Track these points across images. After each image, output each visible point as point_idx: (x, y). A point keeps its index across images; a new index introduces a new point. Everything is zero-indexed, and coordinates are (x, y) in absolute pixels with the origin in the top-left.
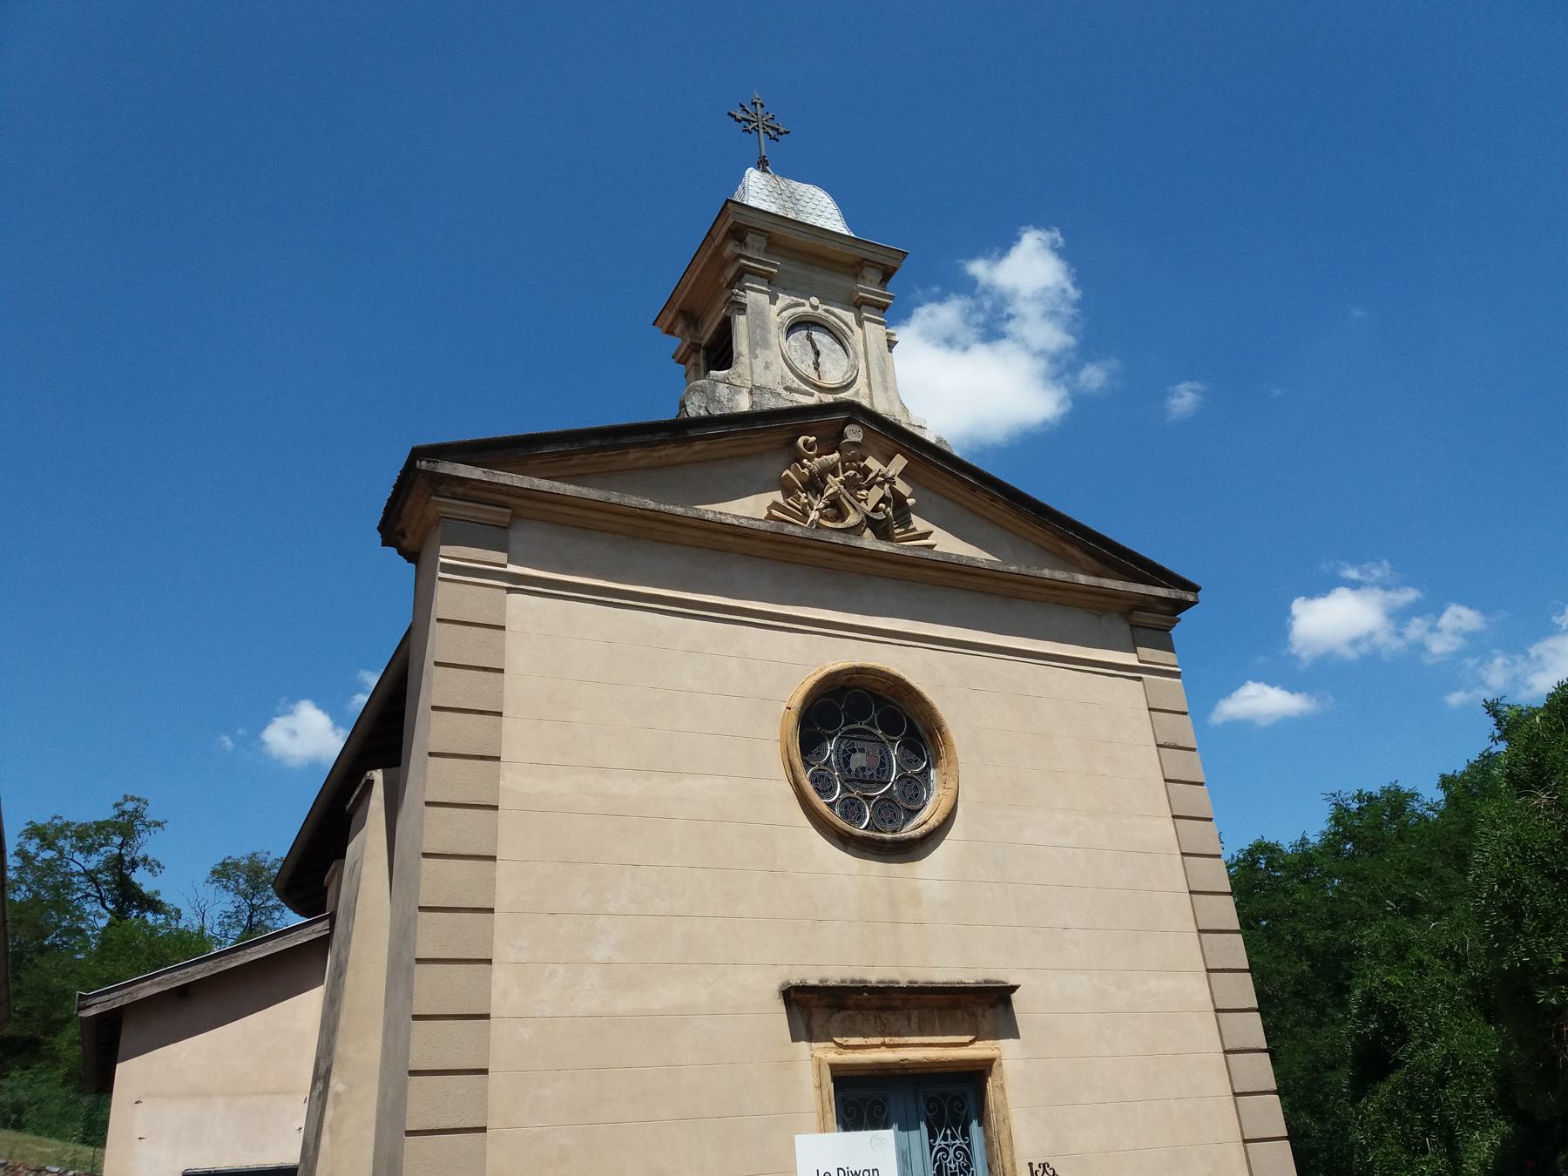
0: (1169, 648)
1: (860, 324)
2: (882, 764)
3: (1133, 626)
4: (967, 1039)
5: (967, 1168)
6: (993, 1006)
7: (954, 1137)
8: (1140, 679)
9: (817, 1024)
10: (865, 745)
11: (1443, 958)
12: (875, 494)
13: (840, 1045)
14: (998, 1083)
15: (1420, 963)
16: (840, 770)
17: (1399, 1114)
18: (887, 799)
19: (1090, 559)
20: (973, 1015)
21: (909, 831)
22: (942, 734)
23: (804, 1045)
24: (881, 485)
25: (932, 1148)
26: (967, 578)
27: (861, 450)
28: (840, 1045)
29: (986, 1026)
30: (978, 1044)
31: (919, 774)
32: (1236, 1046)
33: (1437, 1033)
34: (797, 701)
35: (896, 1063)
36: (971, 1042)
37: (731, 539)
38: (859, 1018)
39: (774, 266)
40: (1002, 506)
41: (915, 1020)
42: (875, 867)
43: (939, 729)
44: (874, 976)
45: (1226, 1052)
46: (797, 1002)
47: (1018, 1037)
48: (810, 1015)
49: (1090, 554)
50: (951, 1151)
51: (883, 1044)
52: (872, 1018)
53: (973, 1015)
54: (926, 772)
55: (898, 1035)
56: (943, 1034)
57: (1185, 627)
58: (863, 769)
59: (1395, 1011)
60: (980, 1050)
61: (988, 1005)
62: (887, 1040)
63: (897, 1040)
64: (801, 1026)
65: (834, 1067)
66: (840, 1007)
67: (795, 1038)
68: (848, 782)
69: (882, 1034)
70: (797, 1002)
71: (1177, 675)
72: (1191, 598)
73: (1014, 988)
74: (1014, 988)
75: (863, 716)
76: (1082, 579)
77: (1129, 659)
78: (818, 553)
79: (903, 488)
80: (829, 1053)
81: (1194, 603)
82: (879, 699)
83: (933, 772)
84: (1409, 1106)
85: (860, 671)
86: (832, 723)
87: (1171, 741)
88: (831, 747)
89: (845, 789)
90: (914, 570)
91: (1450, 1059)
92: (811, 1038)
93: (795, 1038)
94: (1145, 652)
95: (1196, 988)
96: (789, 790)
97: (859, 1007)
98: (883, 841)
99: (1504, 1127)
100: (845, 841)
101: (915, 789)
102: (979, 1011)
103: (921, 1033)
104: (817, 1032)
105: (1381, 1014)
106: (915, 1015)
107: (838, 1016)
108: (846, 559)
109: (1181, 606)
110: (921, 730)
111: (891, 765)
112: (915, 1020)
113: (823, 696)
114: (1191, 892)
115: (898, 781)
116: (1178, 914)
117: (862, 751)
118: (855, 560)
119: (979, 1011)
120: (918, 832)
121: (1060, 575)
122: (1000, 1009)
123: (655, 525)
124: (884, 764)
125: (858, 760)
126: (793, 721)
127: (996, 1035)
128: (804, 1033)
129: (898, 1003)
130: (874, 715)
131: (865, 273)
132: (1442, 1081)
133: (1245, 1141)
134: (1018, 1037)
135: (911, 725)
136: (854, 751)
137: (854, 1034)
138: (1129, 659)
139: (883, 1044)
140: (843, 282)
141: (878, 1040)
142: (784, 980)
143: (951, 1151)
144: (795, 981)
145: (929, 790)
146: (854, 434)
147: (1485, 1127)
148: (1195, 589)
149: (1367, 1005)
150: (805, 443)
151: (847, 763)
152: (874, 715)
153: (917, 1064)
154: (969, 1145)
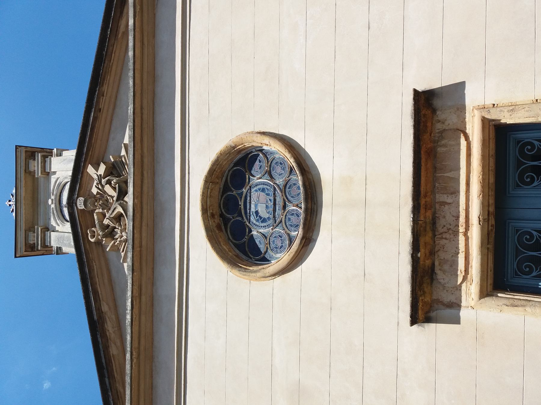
1: (55, 173)
9: (447, 297)
12: (108, 189)
13: (465, 278)
23: (463, 313)
24: (103, 186)
26: (145, 116)
27: (89, 196)
28: (465, 278)
29: (452, 120)
30: (469, 131)
37: (143, 298)
39: (38, 229)
40: (105, 88)
42: (327, 217)
47: (461, 86)
48: (438, 301)
51: (466, 234)
52: (443, 242)
55: (458, 217)
56: (458, 169)
61: (432, 114)
62: (462, 229)
63: (462, 219)
64: (448, 312)
65: (484, 294)
67: (457, 321)
69: (456, 233)
74: (415, 91)
78: (144, 235)
79: (102, 168)
80: (470, 291)
85: (204, 210)
90: (146, 160)
92: (457, 305)
93: (457, 321)
96: (279, 280)
97: (432, 253)
102: (439, 126)
103: (456, 192)
107: (440, 275)
108: (145, 211)
118: (145, 207)
119: (439, 126)
122: (437, 103)
123: (142, 348)
127: (461, 108)
129: (429, 214)
131: (32, 171)
134: (461, 86)
137: (455, 263)
139: (466, 234)
140: (42, 181)
141: (462, 239)
144: (409, 319)
146: (80, 203)
150: (93, 236)
153: (484, 205)
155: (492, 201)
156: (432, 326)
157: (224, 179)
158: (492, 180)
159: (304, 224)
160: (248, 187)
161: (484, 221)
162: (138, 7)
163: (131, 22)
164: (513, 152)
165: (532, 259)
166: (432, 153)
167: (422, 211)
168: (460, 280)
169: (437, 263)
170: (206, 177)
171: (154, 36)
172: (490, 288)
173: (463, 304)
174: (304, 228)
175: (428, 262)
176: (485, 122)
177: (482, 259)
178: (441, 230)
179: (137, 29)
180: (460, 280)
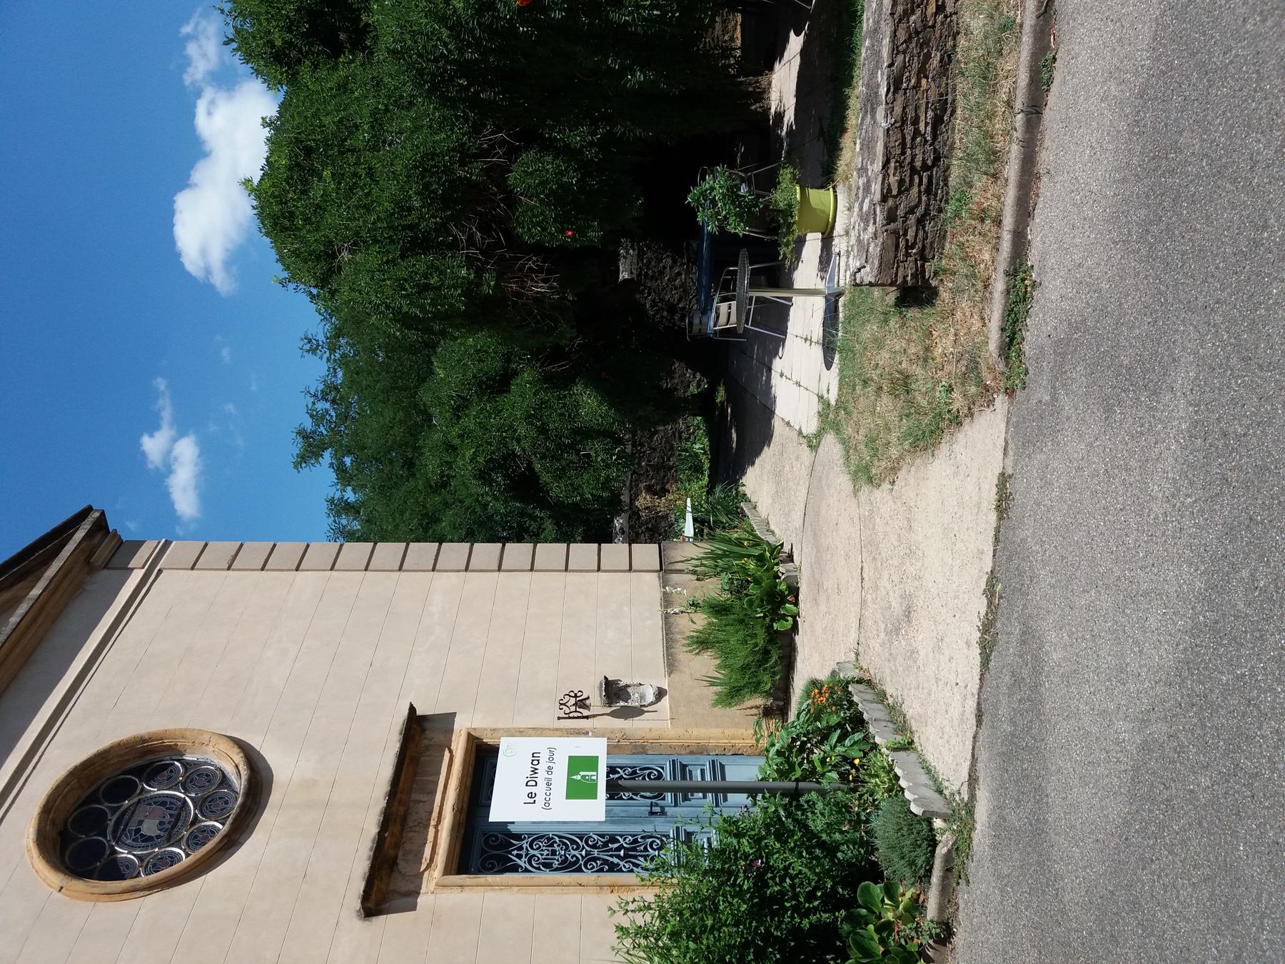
0: (138, 545)
2: (163, 804)
3: (106, 566)
4: (447, 754)
5: (549, 839)
6: (424, 730)
7: (521, 848)
8: (160, 571)
9: (403, 886)
10: (136, 818)
11: (459, 417)
13: (429, 866)
14: (489, 733)
15: (461, 436)
16: (153, 847)
17: (563, 469)
18: (200, 804)
19: (19, 586)
20: (427, 748)
21: (239, 783)
22: (150, 739)
23: (421, 900)
25: (527, 871)
28: (429, 866)
31: (186, 770)
32: (497, 562)
33: (511, 427)
34: (55, 878)
35: (455, 816)
36: (451, 752)
38: (408, 846)
41: (421, 797)
42: (268, 818)
43: (144, 741)
44: (372, 829)
45: (499, 570)
46: (379, 903)
49: (12, 585)
50: (532, 852)
51: (436, 827)
52: (410, 835)
53: (427, 748)
54: (186, 765)
57: (125, 526)
58: (161, 823)
59: (491, 459)
60: (459, 745)
61: (421, 736)
62: (433, 823)
63: (435, 814)
65: (447, 871)
66: (393, 863)
67: (413, 908)
68: (171, 839)
70: (379, 903)
71: (167, 544)
72: (97, 515)
73: (412, 709)
74: (412, 709)
75: (102, 816)
76: (36, 592)
77: (137, 575)
80: (433, 877)
81: (103, 513)
82: (93, 798)
83: (188, 757)
84: (558, 460)
85: (47, 810)
86: (98, 850)
87: (229, 558)
88: (123, 853)
89: (177, 844)
91: (529, 418)
93: (413, 908)
94: (136, 561)
95: (444, 581)
96: (157, 897)
97: (397, 846)
98: (243, 805)
99: (578, 388)
100: (231, 843)
101: (199, 776)
102: (426, 742)
103: (434, 792)
104: (412, 887)
105: (491, 470)
106: (415, 796)
107: (402, 865)
109: (101, 526)
110: (139, 763)
111: (167, 796)
112: (421, 797)
113: (62, 855)
114: (366, 570)
115: (186, 791)
116: (381, 583)
117: (141, 822)
120: (243, 768)
121: (22, 609)
122: (426, 725)
124: (163, 802)
125: (150, 828)
126: (79, 885)
127: (450, 731)
128: (410, 899)
129: (402, 809)
130: (104, 806)
132: (543, 431)
133: (566, 570)
135: (131, 772)
136: (138, 831)
138: (137, 575)
139: (436, 827)
141: (431, 831)
142: (354, 914)
143: (532, 852)
145: (206, 763)
147: (577, 405)
148: (89, 510)
149: (484, 478)
151: (150, 839)
152: (104, 806)
153: (460, 797)
154: (530, 835)
155: (465, 806)
156: (383, 917)
157: (94, 788)
158: (469, 783)
159: (235, 820)
160: (136, 800)
161: (458, 811)
162: (52, 586)
163: (36, 592)
164: (479, 842)
165: (493, 857)
166: (415, 761)
167: (396, 804)
168: (423, 867)
169: (400, 854)
170: (76, 768)
171: (54, 622)
172: (455, 866)
173: (422, 891)
174: (232, 824)
175: (392, 852)
176: (471, 738)
177: (448, 857)
178: (410, 824)
179: (38, 604)
180: (423, 867)
